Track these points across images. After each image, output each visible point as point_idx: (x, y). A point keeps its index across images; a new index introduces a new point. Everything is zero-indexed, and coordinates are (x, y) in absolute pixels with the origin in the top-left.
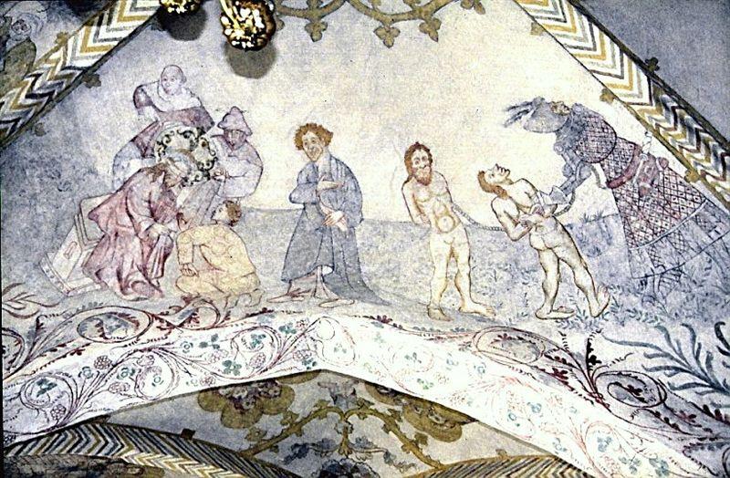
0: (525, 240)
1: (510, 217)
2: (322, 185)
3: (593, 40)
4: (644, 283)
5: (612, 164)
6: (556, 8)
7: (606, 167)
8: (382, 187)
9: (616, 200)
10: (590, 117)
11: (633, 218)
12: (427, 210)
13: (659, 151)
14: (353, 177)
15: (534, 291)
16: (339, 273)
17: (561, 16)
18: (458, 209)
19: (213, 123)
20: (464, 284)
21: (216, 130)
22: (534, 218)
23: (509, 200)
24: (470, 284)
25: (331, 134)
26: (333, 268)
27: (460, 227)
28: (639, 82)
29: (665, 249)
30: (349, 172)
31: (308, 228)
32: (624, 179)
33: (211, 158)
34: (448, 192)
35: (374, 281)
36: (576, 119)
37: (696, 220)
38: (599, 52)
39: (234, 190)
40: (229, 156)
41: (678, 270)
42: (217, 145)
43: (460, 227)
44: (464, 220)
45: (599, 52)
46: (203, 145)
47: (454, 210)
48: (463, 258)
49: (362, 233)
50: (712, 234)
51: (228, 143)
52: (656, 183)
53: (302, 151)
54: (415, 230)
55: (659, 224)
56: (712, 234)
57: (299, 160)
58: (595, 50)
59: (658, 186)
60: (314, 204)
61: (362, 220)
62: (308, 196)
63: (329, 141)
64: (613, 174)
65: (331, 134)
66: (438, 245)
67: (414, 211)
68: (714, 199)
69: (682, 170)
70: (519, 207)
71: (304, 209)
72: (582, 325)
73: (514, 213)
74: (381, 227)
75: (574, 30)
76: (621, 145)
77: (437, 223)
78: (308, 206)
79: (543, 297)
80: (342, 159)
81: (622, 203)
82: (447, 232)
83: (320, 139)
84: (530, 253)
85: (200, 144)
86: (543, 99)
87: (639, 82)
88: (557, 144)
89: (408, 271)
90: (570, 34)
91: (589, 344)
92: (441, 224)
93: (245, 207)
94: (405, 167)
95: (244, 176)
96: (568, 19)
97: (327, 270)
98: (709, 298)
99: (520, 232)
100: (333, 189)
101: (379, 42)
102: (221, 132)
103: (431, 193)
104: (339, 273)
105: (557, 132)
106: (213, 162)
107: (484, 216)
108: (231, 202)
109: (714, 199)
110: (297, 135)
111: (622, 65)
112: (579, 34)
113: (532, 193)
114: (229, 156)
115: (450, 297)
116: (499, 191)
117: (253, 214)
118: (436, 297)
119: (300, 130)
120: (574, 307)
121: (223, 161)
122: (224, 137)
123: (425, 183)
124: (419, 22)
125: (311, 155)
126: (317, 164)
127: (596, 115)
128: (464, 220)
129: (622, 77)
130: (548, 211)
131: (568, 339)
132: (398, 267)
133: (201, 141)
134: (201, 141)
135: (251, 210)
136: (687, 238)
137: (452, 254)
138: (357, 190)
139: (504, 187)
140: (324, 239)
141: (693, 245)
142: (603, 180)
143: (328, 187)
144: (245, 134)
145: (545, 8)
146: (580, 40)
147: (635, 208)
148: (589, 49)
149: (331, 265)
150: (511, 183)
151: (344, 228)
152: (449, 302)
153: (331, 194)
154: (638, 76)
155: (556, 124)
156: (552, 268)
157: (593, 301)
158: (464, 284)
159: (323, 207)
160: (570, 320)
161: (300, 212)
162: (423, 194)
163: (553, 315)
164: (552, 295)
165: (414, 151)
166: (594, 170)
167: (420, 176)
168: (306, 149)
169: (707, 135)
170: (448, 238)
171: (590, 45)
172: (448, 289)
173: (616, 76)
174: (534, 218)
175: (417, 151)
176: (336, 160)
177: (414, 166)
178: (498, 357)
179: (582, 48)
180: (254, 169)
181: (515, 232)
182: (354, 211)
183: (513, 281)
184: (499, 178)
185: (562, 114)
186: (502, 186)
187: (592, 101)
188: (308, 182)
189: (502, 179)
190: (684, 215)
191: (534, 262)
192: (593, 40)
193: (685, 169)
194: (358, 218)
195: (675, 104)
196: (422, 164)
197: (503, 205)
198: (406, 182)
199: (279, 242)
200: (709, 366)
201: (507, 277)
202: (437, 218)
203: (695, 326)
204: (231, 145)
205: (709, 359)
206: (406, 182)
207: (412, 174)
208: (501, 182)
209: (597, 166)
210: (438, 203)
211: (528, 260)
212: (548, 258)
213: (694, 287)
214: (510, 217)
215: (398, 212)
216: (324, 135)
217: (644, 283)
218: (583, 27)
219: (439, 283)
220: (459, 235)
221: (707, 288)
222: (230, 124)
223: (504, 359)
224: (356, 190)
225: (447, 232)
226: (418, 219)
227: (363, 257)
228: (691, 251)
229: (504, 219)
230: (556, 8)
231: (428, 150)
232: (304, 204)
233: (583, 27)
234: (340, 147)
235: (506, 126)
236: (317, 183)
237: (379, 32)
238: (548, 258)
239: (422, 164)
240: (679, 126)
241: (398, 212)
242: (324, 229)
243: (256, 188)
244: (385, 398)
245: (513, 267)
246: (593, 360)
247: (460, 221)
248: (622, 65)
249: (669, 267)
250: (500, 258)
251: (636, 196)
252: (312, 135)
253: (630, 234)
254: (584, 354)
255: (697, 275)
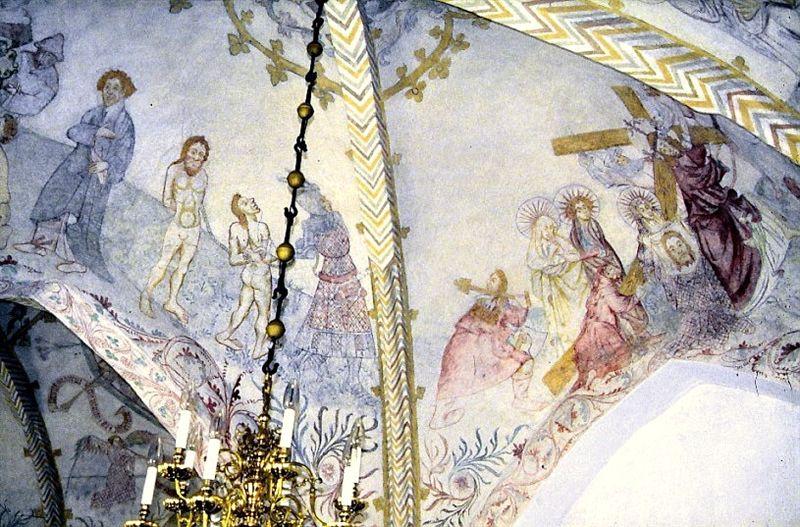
0: (239, 269)
1: (239, 245)
2: (103, 131)
3: (381, 211)
4: (298, 352)
5: (332, 265)
6: (374, 175)
7: (327, 263)
8: (151, 161)
9: (318, 288)
10: (342, 227)
11: (320, 308)
12: (179, 198)
13: (366, 284)
14: (133, 136)
15: (224, 317)
16: (82, 226)
17: (373, 183)
18: (204, 212)
19: (31, 40)
20: (177, 283)
21: (32, 48)
22: (255, 257)
23: (245, 231)
24: (181, 285)
25: (133, 89)
26: (78, 218)
27: (197, 229)
28: (387, 255)
29: (325, 340)
30: (131, 130)
31: (71, 170)
32: (332, 280)
33: (12, 69)
34: (204, 193)
35: (107, 246)
36: (332, 220)
37: (356, 337)
38: (378, 220)
39: (19, 106)
40: (30, 73)
41: (324, 359)
42: (24, 61)
43: (197, 229)
44: (204, 225)
45: (378, 220)
46: (10, 57)
47: (200, 213)
48: (186, 259)
49: (117, 190)
50: (359, 353)
51: (36, 61)
52: (350, 299)
53: (100, 92)
54: (161, 211)
55: (333, 323)
56: (359, 353)
57: (94, 100)
58: (377, 217)
59: (349, 301)
60: (87, 146)
61: (122, 179)
62: (84, 137)
63: (130, 95)
64: (328, 271)
65: (133, 89)
66: (173, 235)
67: (168, 194)
68: (376, 340)
69: (370, 306)
70: (250, 241)
71: (76, 148)
72: (243, 361)
73: (243, 244)
74: (135, 193)
75: (374, 196)
76: (346, 260)
77: (181, 214)
78: (81, 147)
79: (228, 324)
80: (132, 115)
81: (320, 293)
82: (184, 227)
83: (123, 88)
84: (237, 282)
85: (7, 56)
86: (319, 189)
87: (387, 255)
88: (307, 222)
89: (140, 248)
90: (370, 196)
91: (239, 379)
92: (184, 218)
93: (23, 128)
94: (180, 150)
95: (34, 95)
96: (376, 188)
97: (72, 220)
98: (329, 388)
99: (239, 261)
100: (111, 139)
101: (226, 45)
102: (35, 49)
103: (189, 185)
104: (82, 226)
105: (313, 216)
106: (12, 73)
107: (219, 229)
108: (12, 117)
109: (376, 340)
110: (103, 77)
111: (385, 238)
112: (375, 201)
113: (265, 238)
114: (30, 73)
115: (161, 291)
116: (242, 219)
117: (27, 136)
118: (151, 286)
119: (109, 73)
120: (244, 344)
121: (22, 76)
122: (35, 55)
123: (190, 173)
124: (270, 61)
125: (107, 101)
126: (107, 110)
127: (345, 230)
128: (204, 225)
129: (379, 244)
130: (268, 258)
131: (228, 368)
132: (132, 241)
133: (10, 53)
134: (10, 53)
135: (27, 132)
136: (343, 343)
137: (180, 250)
138: (131, 149)
139: (248, 218)
140: (82, 185)
141: (343, 350)
142: (319, 269)
143: (106, 138)
144: (56, 59)
145: (372, 208)
146: (374, 206)
147: (326, 302)
148: (374, 214)
149: (77, 215)
150: (255, 220)
151: (102, 181)
152: (160, 296)
153: (106, 143)
154: (389, 251)
155: (316, 210)
156: (245, 304)
157: (259, 346)
158: (177, 283)
159: (93, 154)
160: (237, 352)
161: (72, 150)
162: (182, 182)
163: (228, 343)
164: (234, 326)
165: (197, 142)
166: (318, 259)
167: (190, 165)
168: (105, 91)
169: (400, 306)
170: (183, 233)
171: (376, 212)
172: (163, 282)
173: (376, 241)
174: (255, 257)
175: (199, 144)
176: (127, 113)
177: (189, 154)
178: (176, 375)
179: (370, 210)
180: (46, 93)
181: (237, 258)
182: (119, 167)
183: (213, 299)
184: (248, 209)
185: (324, 208)
186: (247, 217)
187: (350, 222)
188: (91, 123)
189: (250, 211)
190: (351, 330)
191: (237, 291)
192: (381, 211)
193: (373, 307)
194: (118, 176)
195: (397, 276)
196: (197, 157)
197: (239, 232)
198: (175, 163)
199: (40, 174)
200: (302, 433)
201: (210, 290)
202: (183, 210)
203: (310, 400)
204: (37, 64)
205: (305, 428)
206: (175, 163)
207: (184, 159)
208: (248, 214)
209: (322, 258)
210: (190, 197)
211: (231, 287)
212: (247, 294)
213: (326, 375)
214: (239, 245)
215: (155, 187)
216: (128, 87)
217: (298, 352)
218: (380, 200)
219: (158, 273)
220: (192, 236)
221: (333, 381)
222: (47, 46)
223: (180, 379)
224: (129, 148)
225: (184, 227)
226: (168, 203)
227: (108, 216)
228: (339, 353)
229: (234, 243)
230: (374, 175)
231: (207, 149)
232: (78, 143)
233: (380, 200)
234: (136, 105)
235: (280, 180)
236: (99, 127)
237: (231, 38)
238: (247, 294)
239: (197, 157)
240: (389, 295)
241: (155, 187)
242: (85, 175)
243: (41, 110)
244: (34, 131)
245: (219, 287)
246: (236, 395)
247: (200, 223)
248: (385, 238)
249: (320, 352)
250: (213, 273)
251: (332, 296)
252: (117, 83)
253: (311, 316)
254: (233, 386)
255: (332, 370)
